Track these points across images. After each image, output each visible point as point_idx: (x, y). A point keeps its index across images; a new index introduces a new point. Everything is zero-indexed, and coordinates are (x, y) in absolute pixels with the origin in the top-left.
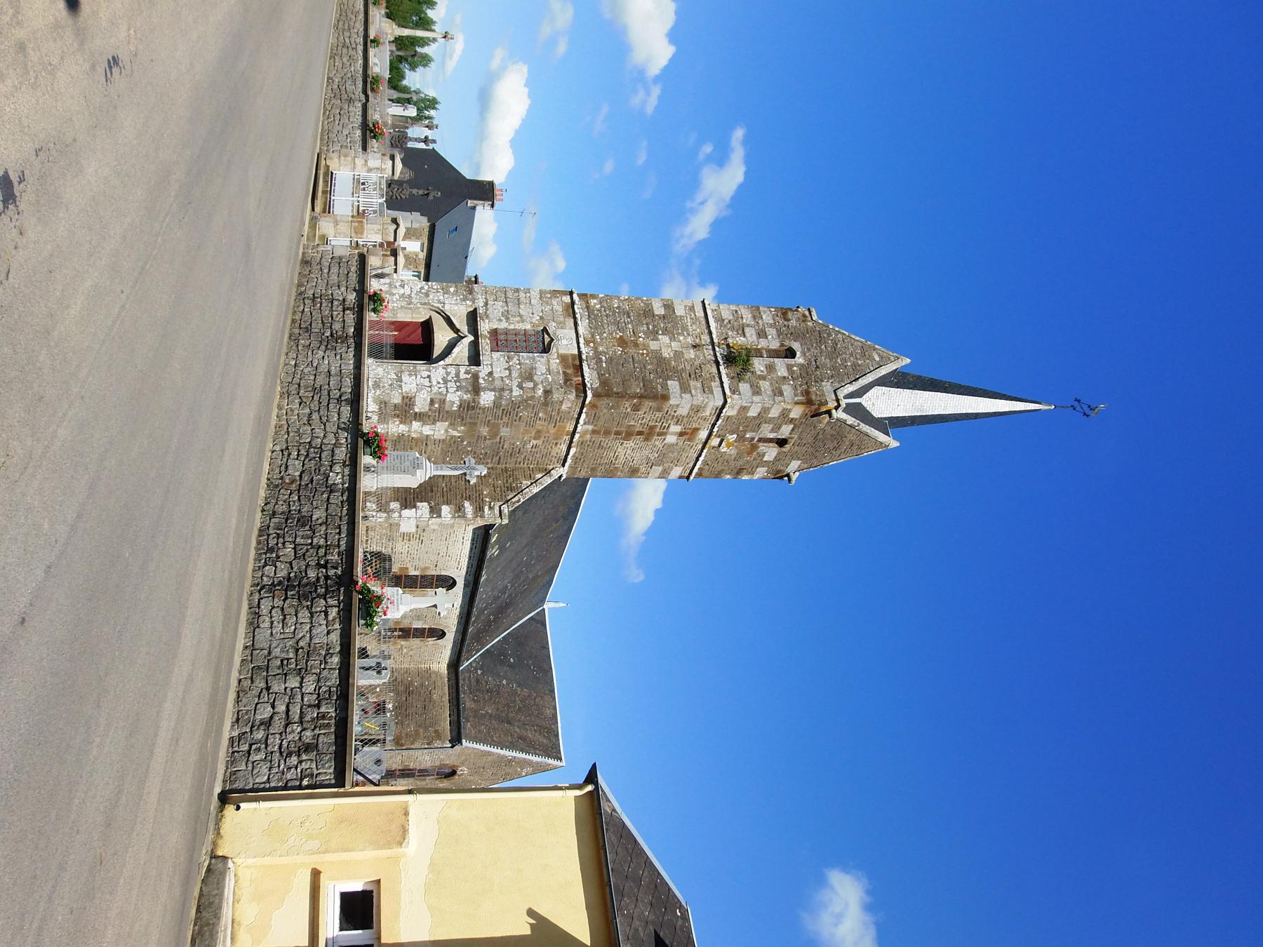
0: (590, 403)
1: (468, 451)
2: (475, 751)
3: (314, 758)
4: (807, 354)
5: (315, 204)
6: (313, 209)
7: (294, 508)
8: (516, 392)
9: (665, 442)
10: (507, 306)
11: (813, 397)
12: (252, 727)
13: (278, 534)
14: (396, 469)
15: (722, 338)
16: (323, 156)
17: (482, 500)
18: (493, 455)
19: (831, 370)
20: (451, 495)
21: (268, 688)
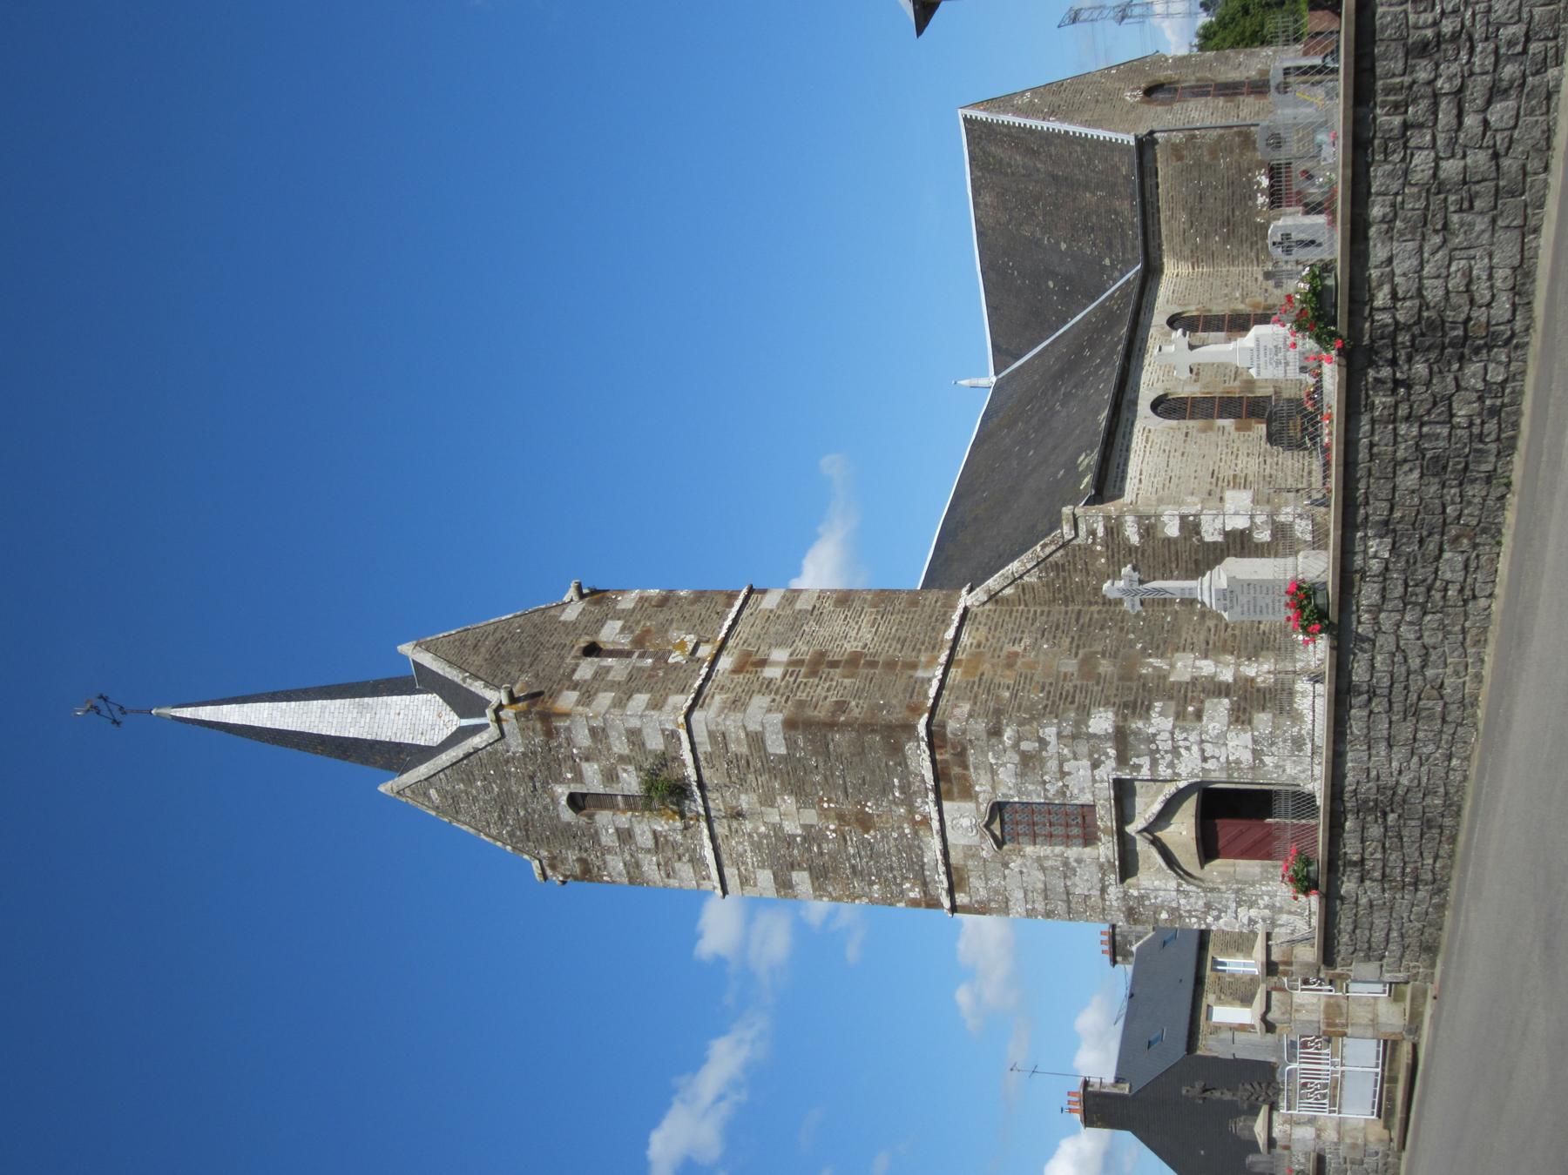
0: (921, 715)
1: (1133, 633)
2: (1112, 127)
3: (1412, 31)
4: (548, 800)
5: (1410, 1056)
6: (1415, 1047)
7: (1453, 491)
8: (1050, 733)
9: (790, 650)
10: (1066, 886)
11: (539, 726)
12: (1523, 85)
13: (1481, 441)
14: (1264, 589)
15: (693, 829)
16: (1395, 1145)
17: (1108, 547)
18: (1089, 626)
19: (510, 772)
20: (1164, 555)
21: (1496, 156)
